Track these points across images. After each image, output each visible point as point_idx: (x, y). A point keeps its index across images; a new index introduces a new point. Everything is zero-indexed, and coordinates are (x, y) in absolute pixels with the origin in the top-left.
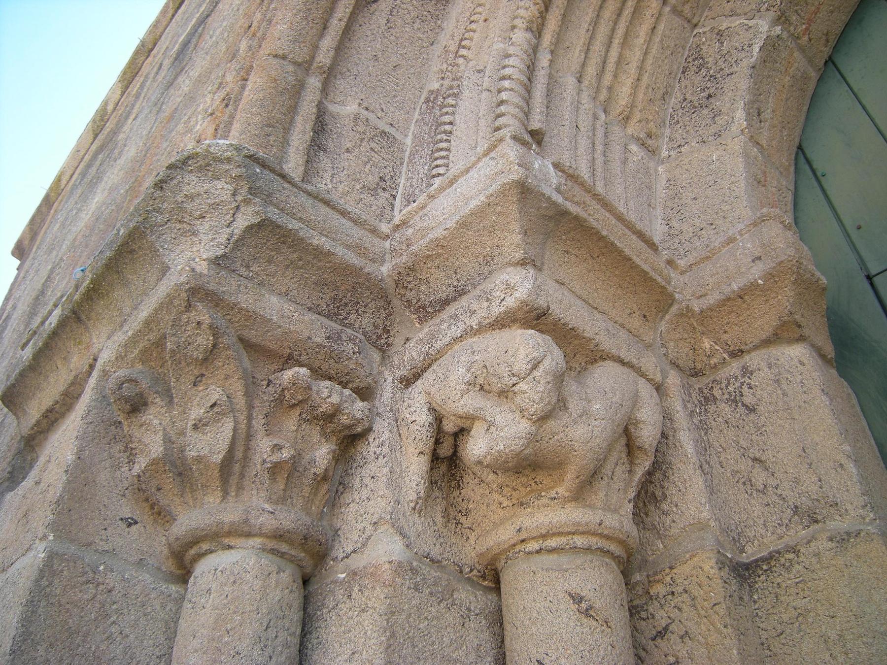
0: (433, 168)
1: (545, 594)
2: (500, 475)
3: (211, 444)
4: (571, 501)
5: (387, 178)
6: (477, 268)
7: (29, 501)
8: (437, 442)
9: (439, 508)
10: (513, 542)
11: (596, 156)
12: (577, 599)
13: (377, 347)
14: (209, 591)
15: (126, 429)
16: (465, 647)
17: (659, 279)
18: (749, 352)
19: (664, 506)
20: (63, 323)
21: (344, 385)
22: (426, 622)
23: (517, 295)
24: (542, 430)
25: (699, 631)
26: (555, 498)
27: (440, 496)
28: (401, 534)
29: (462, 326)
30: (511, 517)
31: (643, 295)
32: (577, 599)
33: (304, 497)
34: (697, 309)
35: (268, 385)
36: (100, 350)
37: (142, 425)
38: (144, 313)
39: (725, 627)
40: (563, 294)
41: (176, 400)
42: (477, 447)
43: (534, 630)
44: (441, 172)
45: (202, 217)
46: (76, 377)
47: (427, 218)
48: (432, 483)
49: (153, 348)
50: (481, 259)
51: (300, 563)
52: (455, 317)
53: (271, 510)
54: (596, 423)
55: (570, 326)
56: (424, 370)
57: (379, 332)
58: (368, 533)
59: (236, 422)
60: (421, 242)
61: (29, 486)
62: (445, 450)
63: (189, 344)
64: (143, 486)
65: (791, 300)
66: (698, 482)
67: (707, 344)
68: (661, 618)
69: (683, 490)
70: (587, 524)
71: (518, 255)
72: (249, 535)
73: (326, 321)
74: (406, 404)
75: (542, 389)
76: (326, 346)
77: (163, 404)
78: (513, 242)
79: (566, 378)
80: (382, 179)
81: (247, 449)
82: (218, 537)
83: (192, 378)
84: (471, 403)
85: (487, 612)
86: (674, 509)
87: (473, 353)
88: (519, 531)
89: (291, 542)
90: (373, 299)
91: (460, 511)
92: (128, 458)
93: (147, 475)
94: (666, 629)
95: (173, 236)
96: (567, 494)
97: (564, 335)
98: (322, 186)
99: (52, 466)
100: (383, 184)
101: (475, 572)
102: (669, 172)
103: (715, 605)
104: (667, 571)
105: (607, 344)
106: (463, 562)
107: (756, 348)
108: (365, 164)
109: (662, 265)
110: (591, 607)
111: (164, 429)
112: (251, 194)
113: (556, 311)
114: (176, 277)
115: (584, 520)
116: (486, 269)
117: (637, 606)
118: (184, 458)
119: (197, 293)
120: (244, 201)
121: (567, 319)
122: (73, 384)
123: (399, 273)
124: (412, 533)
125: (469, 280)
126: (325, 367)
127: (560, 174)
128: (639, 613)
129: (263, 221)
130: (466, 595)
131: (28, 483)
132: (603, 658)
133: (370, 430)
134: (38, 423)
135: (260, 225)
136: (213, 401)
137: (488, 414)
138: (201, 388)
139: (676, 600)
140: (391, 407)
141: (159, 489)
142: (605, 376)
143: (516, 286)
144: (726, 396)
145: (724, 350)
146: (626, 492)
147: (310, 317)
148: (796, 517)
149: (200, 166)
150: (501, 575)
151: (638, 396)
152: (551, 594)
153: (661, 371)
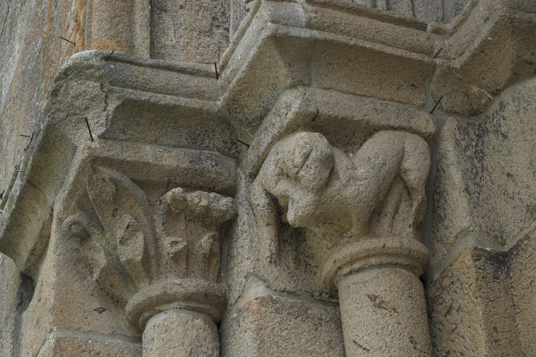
1: (354, 299)
3: (133, 251)
7: (37, 313)
9: (291, 257)
10: (334, 270)
12: (373, 298)
13: (231, 157)
14: (153, 339)
15: (83, 253)
16: (318, 343)
18: (503, 90)
19: (446, 223)
20: (24, 191)
21: (210, 190)
22: (287, 331)
23: (293, 110)
24: (323, 196)
27: (291, 249)
28: (262, 280)
29: (271, 135)
32: (373, 298)
33: (201, 270)
34: (458, 66)
35: (160, 204)
36: (53, 204)
37: (91, 249)
38: (71, 178)
41: (106, 229)
43: (351, 322)
45: (87, 108)
46: (44, 224)
49: (80, 201)
51: (208, 312)
52: (266, 129)
53: (179, 283)
54: (361, 183)
55: (340, 118)
58: (243, 284)
59: (145, 234)
61: (35, 304)
63: (102, 193)
64: (102, 287)
65: (515, 47)
67: (475, 89)
69: (454, 209)
70: (374, 249)
71: (289, 81)
72: (170, 302)
73: (188, 150)
75: (313, 172)
76: (191, 169)
77: (99, 232)
78: (282, 73)
80: (214, 19)
81: (157, 248)
82: (153, 307)
83: (111, 213)
87: (277, 154)
88: (335, 262)
89: (198, 301)
91: (308, 256)
92: (89, 270)
93: (102, 279)
95: (74, 125)
96: (357, 232)
98: (169, 42)
99: (44, 287)
100: (216, 23)
101: (324, 295)
104: (449, 267)
105: (376, 119)
106: (314, 289)
107: (507, 86)
108: (198, 12)
110: (383, 302)
111: (104, 248)
112: (112, 85)
114: (80, 157)
115: (373, 246)
118: (120, 263)
119: (94, 162)
120: (109, 91)
122: (43, 229)
123: (228, 104)
124: (271, 278)
125: (269, 101)
126: (195, 182)
129: (124, 101)
130: (316, 310)
131: (34, 302)
133: (236, 215)
134: (28, 260)
135: (123, 104)
136: (127, 224)
138: (118, 217)
140: (246, 197)
141: (112, 286)
144: (493, 128)
145: (488, 92)
147: (175, 152)
148: (529, 213)
149: (76, 74)
152: (358, 298)
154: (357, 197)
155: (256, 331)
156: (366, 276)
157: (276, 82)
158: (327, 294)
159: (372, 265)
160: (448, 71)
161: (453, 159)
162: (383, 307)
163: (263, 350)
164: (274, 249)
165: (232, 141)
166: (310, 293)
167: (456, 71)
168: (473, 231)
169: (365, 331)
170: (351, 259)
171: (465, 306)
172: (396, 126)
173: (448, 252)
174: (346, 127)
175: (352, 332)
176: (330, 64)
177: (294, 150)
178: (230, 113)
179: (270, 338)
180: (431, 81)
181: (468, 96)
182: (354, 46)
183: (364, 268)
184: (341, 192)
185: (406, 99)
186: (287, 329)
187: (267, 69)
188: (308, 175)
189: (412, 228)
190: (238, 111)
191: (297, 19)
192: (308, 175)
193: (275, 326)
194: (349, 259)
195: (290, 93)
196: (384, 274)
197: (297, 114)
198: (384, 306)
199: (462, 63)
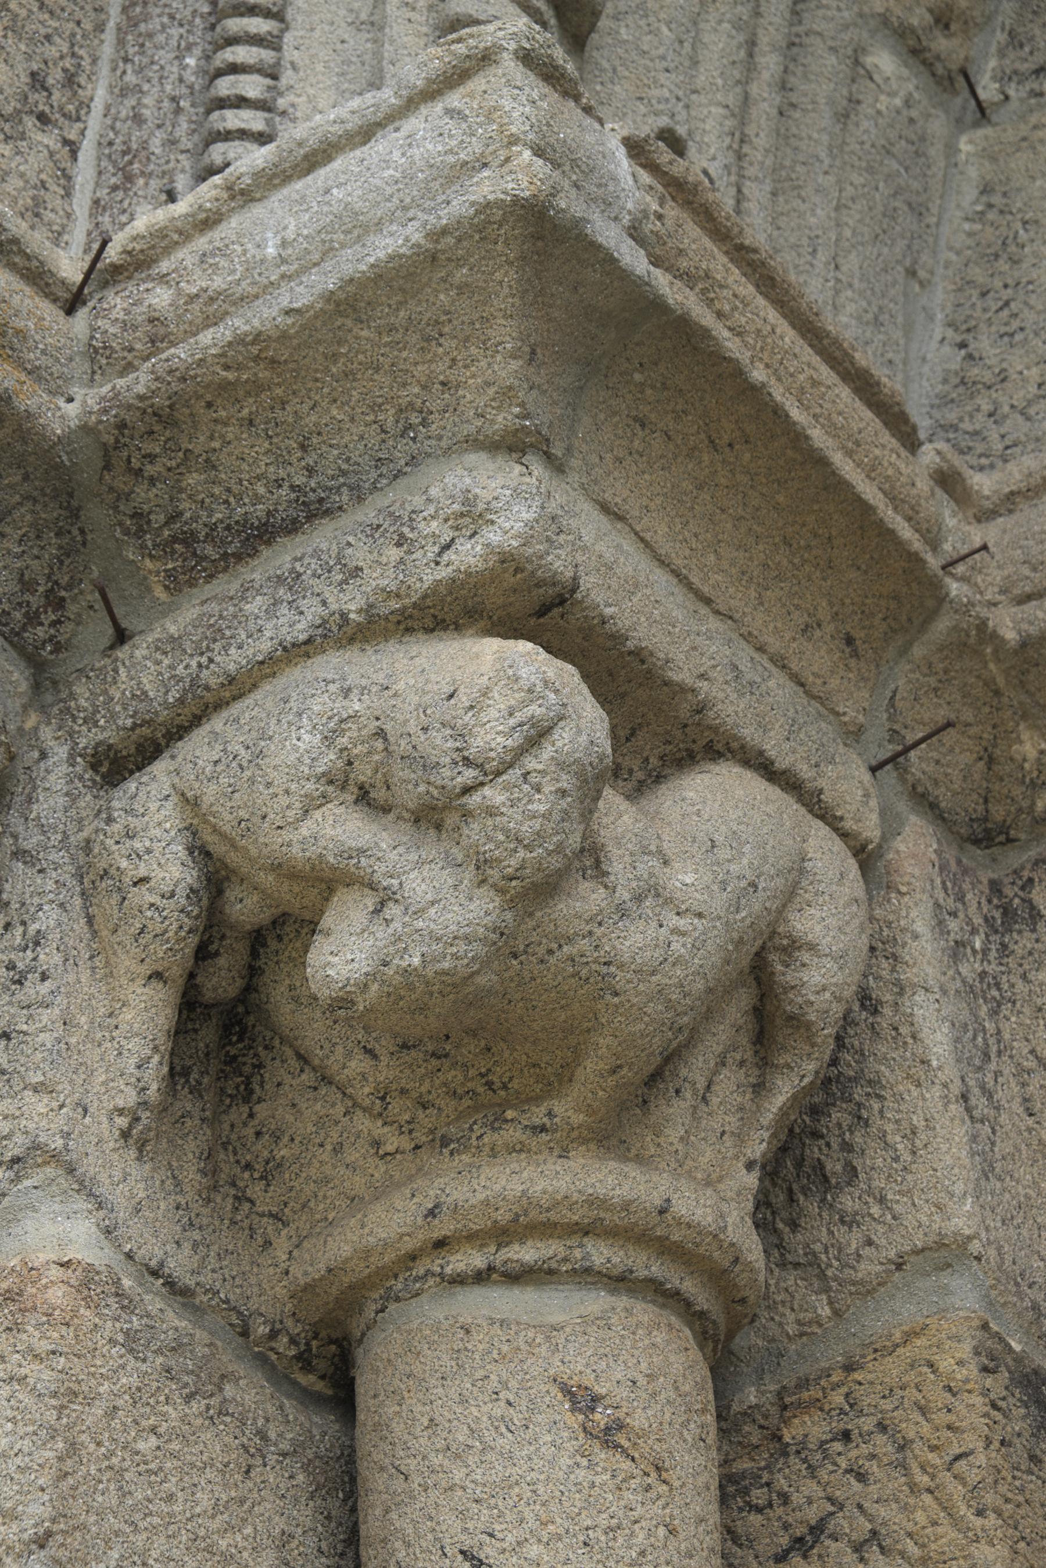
0: (219, 73)
2: (384, 1060)
4: (585, 1141)
5: (55, 76)
6: (373, 441)
8: (203, 953)
9: (191, 1146)
10: (409, 1245)
11: (754, 89)
12: (582, 1400)
13: (21, 650)
16: (248, 1530)
17: (906, 532)
19: (848, 1202)
22: (153, 1441)
23: (493, 536)
24: (531, 924)
25: (910, 1527)
26: (543, 1129)
27: (196, 1113)
29: (312, 611)
30: (411, 1178)
31: (853, 574)
32: (582, 1400)
34: (1010, 635)
39: (980, 1513)
40: (618, 547)
42: (344, 954)
44: (252, 93)
47: (223, 263)
48: (176, 1074)
50: (388, 417)
54: (682, 923)
56: (178, 732)
57: (35, 601)
60: (206, 337)
62: (222, 981)
66: (951, 1145)
68: (807, 1497)
70: (626, 1206)
71: (503, 419)
74: (116, 827)
75: (542, 808)
78: (494, 370)
79: (608, 792)
80: (37, 81)
84: (339, 829)
85: (310, 1453)
86: (875, 1210)
87: (346, 692)
88: (432, 1213)
90: (27, 497)
91: (248, 1166)
94: (817, 1529)
96: (577, 1119)
97: (614, 668)
100: (37, 97)
102: (993, 159)
103: (957, 1458)
105: (732, 710)
109: (924, 484)
110: (621, 1426)
113: (595, 590)
116: (402, 450)
117: (743, 1475)
121: (623, 623)
123: (122, 426)
124: (119, 1197)
125: (344, 473)
127: (646, 178)
128: (745, 1492)
132: (642, 1553)
137: (381, 868)
139: (854, 1453)
140: (66, 836)
142: (712, 801)
143: (500, 506)
146: (740, 1137)
150: (359, 1353)
151: (802, 871)
152: (513, 1384)
153: (883, 814)
154: (653, 973)
155: (54, 1395)
156: (556, 1305)
157: (435, 405)
158: (293, 1341)
159: (588, 1271)
160: (972, 641)
161: (930, 970)
162: (617, 1446)
163: (74, 1488)
164: (154, 1086)
165: (52, 590)
166: (240, 1313)
167: (996, 652)
168: (978, 1258)
169: (532, 1523)
170: (516, 1220)
171: (910, 1535)
172: (781, 764)
173: (837, 1313)
174: (623, 695)
175: (462, 1514)
176: (643, 426)
177: (485, 693)
178: (107, 467)
179: (99, 1444)
180: (904, 651)
181: (991, 761)
182: (755, 391)
183: (551, 1272)
184: (599, 931)
185: (819, 681)
186: (153, 1430)
187: (414, 338)
188: (516, 813)
189: (756, 1174)
190: (150, 470)
191: (611, 188)
192: (516, 813)
193: (120, 1403)
194: (509, 1216)
195: (490, 465)
196: (633, 1321)
197: (506, 559)
198: (626, 1444)
199: (1033, 630)
